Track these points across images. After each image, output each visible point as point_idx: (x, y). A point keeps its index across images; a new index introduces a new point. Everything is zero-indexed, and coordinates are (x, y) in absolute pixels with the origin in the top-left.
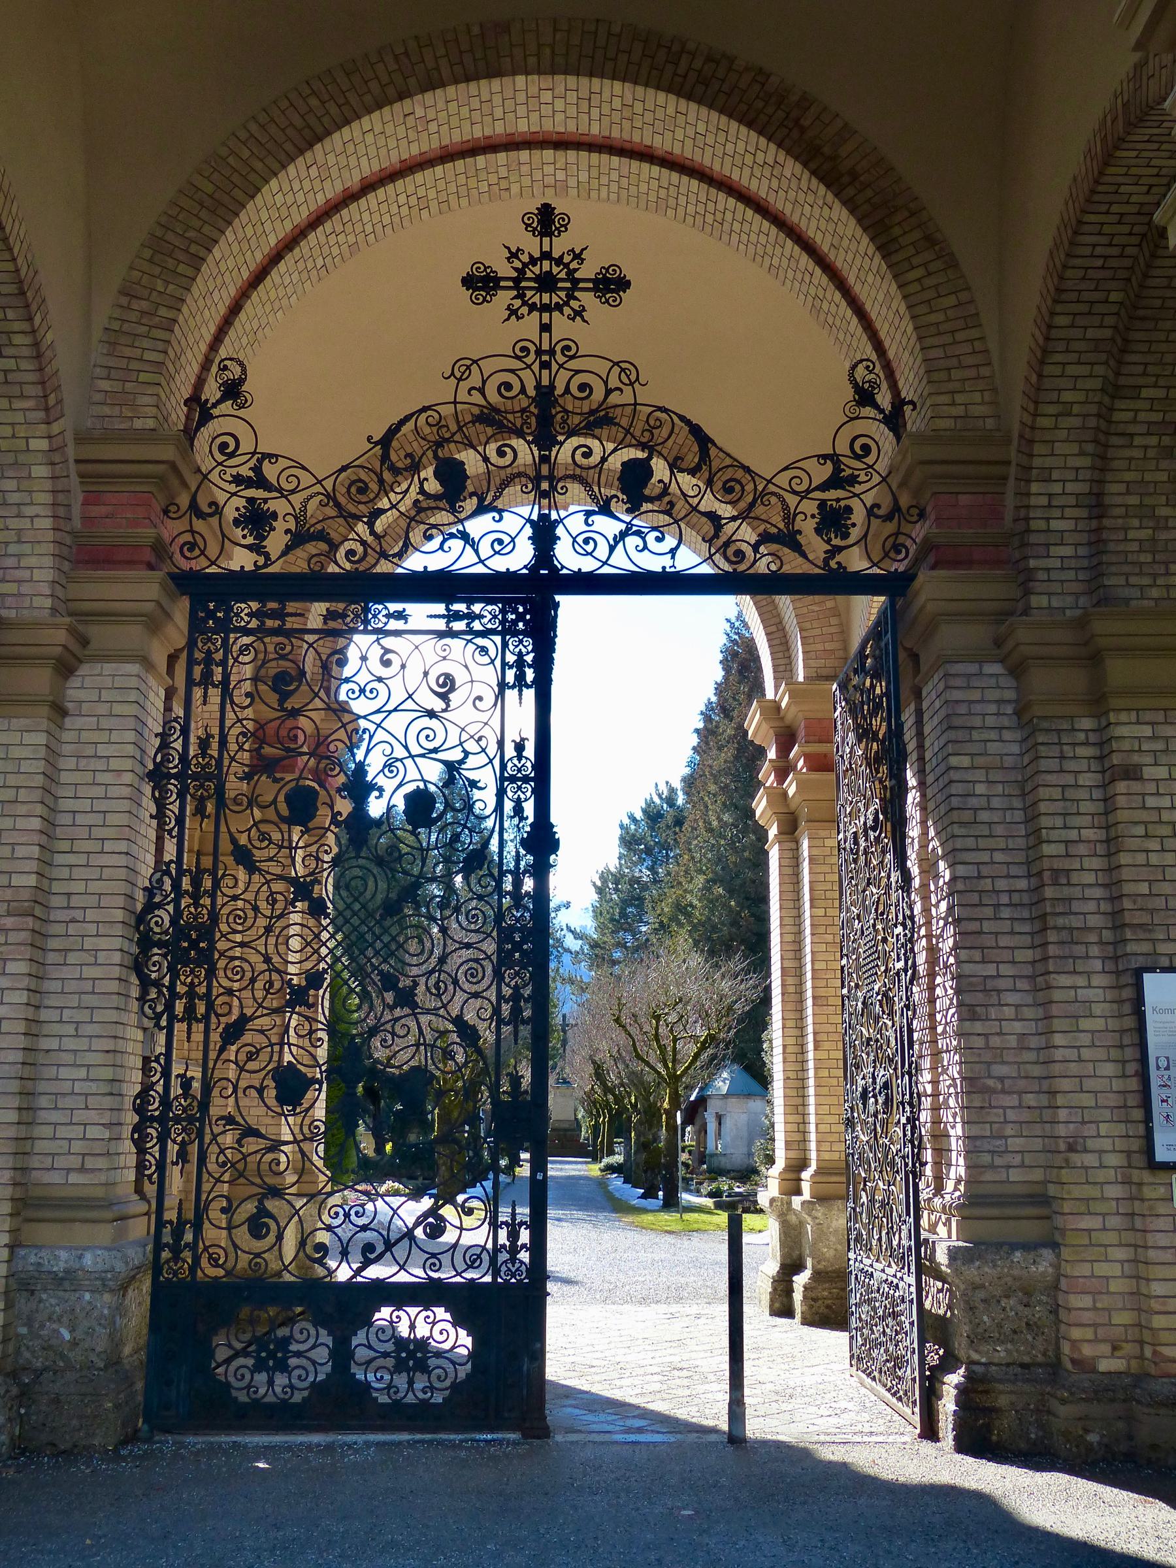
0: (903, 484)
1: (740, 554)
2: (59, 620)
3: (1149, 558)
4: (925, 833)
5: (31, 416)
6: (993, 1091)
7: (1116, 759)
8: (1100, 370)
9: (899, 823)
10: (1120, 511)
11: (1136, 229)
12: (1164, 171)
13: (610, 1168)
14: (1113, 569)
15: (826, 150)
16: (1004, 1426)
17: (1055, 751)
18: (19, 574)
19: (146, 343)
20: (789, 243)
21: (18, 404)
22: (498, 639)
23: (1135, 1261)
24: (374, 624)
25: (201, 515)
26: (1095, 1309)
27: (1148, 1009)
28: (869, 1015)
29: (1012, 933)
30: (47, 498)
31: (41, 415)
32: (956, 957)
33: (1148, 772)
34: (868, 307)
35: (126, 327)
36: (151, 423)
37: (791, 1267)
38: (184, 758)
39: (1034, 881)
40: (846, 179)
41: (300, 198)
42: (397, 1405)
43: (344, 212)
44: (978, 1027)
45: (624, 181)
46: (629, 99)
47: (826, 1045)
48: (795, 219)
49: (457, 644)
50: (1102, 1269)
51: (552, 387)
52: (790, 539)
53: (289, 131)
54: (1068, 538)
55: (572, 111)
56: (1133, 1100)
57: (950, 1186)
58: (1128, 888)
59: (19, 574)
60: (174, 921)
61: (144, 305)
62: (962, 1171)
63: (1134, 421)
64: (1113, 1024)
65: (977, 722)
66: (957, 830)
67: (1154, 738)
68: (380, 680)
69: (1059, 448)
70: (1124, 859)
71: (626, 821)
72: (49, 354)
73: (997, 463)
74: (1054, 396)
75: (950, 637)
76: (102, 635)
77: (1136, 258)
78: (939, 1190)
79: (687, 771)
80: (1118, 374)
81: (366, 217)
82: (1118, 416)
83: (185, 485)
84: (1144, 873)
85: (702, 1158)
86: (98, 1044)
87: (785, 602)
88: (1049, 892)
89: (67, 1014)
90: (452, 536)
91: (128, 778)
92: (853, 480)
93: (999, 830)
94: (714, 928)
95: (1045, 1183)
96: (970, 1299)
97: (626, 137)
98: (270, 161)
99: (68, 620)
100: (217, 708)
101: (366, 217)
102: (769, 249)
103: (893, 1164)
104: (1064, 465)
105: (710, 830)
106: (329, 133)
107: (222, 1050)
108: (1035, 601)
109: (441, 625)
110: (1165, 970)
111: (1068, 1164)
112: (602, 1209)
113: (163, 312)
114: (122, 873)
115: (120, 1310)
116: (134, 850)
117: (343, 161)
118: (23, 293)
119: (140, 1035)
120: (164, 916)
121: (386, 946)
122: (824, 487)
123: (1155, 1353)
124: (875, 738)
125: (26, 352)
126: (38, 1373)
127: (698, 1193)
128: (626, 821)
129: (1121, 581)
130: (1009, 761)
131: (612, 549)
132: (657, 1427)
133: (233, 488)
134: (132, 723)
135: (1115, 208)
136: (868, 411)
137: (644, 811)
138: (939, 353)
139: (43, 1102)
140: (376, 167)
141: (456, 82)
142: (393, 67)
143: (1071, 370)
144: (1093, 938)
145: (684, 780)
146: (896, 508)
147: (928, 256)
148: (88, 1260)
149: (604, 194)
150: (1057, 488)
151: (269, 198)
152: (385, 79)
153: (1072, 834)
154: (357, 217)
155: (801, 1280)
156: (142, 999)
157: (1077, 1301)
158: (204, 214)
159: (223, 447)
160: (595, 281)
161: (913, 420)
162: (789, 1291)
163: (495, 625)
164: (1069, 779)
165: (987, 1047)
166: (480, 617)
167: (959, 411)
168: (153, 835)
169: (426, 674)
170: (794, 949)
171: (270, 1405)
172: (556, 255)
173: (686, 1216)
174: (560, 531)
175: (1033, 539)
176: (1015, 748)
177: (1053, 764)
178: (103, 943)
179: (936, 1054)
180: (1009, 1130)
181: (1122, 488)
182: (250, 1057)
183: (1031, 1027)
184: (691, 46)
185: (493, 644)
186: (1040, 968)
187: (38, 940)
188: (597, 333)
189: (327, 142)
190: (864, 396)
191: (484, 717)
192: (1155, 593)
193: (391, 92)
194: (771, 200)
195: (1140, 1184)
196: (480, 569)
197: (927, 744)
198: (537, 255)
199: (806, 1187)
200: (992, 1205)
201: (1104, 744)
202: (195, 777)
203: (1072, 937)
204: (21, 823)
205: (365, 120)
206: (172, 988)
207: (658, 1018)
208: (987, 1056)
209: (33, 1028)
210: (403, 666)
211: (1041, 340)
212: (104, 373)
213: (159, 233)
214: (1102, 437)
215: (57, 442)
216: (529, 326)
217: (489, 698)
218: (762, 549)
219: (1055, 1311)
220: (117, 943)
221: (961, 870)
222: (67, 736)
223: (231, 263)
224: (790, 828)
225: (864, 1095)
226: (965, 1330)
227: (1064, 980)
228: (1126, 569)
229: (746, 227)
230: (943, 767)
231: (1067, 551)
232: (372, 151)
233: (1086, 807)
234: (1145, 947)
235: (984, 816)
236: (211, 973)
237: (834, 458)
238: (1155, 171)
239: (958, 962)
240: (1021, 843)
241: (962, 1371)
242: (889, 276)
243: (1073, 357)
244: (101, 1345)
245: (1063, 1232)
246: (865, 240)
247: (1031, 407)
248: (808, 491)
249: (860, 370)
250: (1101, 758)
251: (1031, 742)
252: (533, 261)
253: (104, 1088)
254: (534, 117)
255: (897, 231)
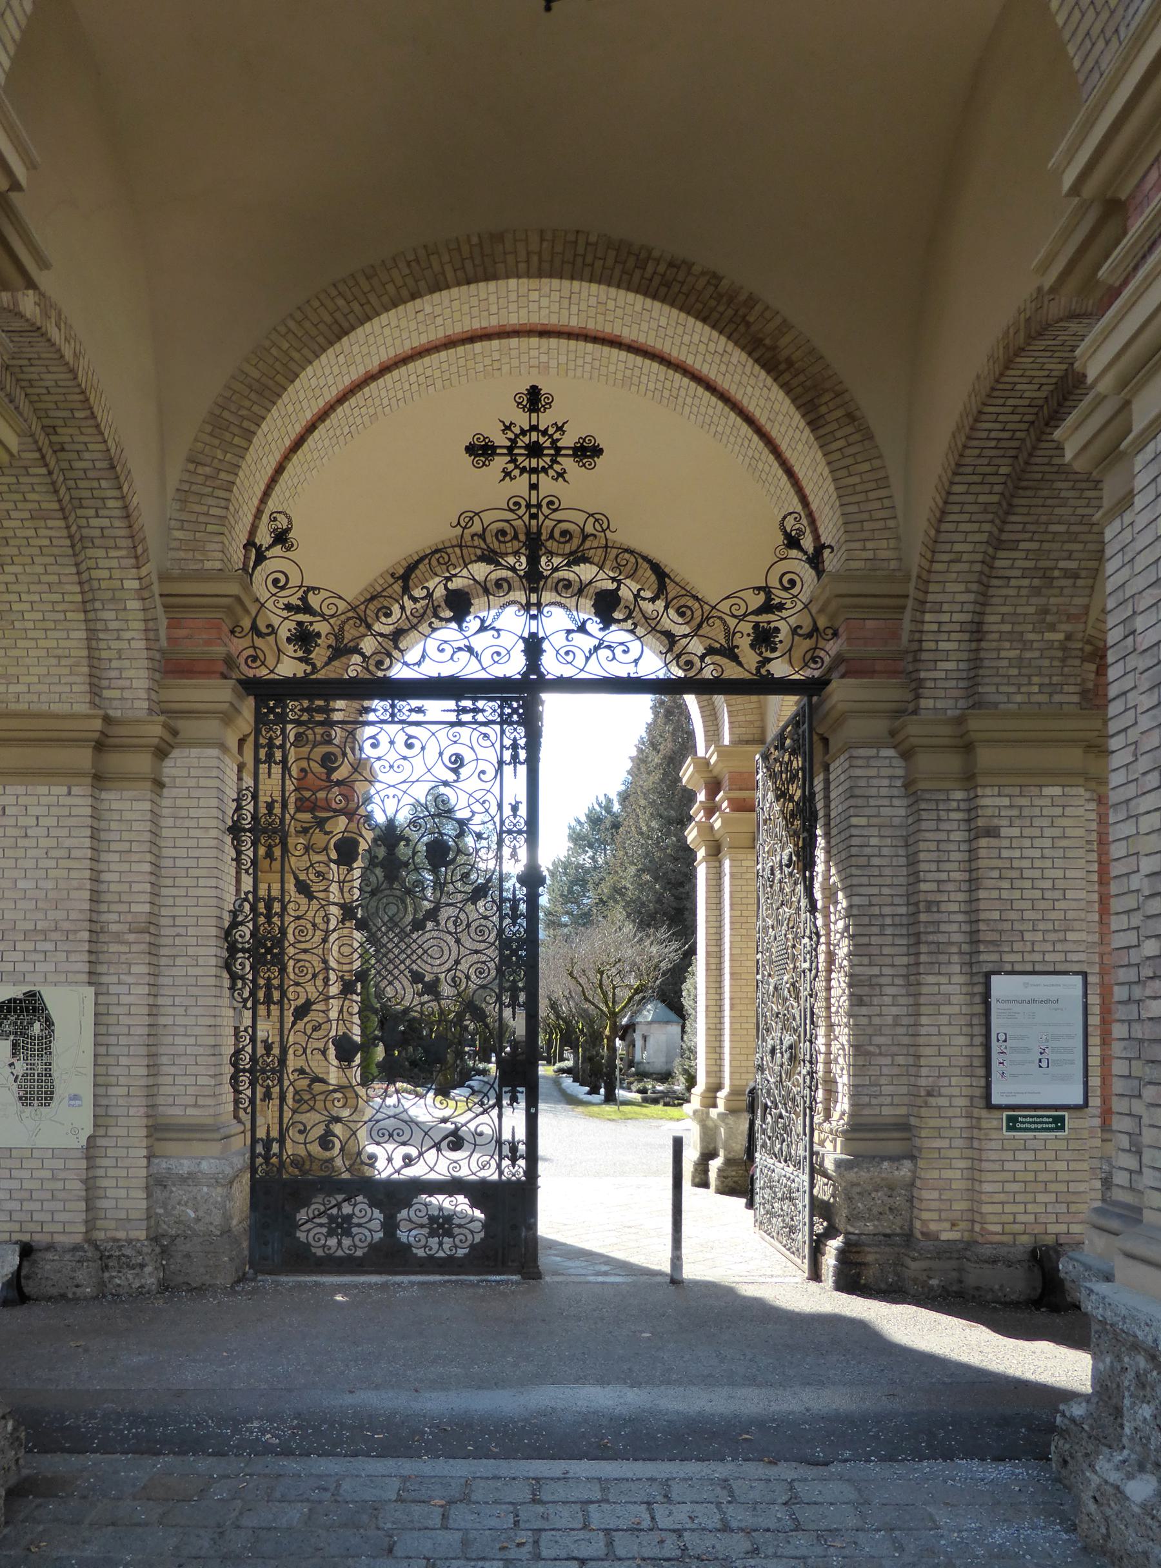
0: (821, 611)
1: (690, 664)
2: (155, 718)
7: (980, 822)
8: (987, 527)
9: (808, 863)
11: (1026, 418)
12: (1054, 373)
13: (562, 1071)
14: (987, 680)
15: (767, 342)
16: (869, 1275)
17: (933, 815)
18: (120, 683)
19: (211, 501)
20: (733, 415)
21: (112, 553)
22: (497, 728)
23: (972, 1169)
24: (399, 717)
25: (260, 634)
26: (940, 1200)
27: (993, 1000)
28: (779, 997)
29: (893, 945)
31: (133, 561)
32: (850, 961)
33: (1004, 832)
35: (194, 488)
36: (218, 565)
37: (708, 1155)
38: (255, 817)
39: (912, 909)
40: (782, 367)
41: (330, 380)
43: (366, 390)
44: (864, 1010)
45: (597, 364)
46: (603, 298)
47: (740, 1007)
48: (739, 397)
49: (464, 732)
51: (539, 533)
52: (730, 653)
53: (321, 326)
54: (953, 656)
55: (555, 307)
56: (977, 1062)
57: (836, 1116)
58: (982, 916)
59: (120, 683)
60: (253, 935)
61: (208, 470)
62: (846, 1107)
63: (1012, 567)
65: (873, 792)
66: (854, 871)
67: (1011, 806)
68: (405, 758)
69: (950, 587)
70: (982, 894)
71: (573, 824)
72: (135, 513)
73: (898, 596)
74: (948, 547)
75: (855, 728)
76: (187, 728)
77: (1023, 440)
78: (828, 1117)
79: (623, 788)
80: (1001, 531)
81: (383, 393)
83: (247, 611)
84: (998, 905)
85: (631, 1064)
86: (201, 1021)
87: (719, 700)
88: (923, 917)
89: (177, 1001)
90: (460, 649)
91: (214, 833)
92: (781, 607)
94: (643, 904)
95: (908, 1115)
97: (599, 328)
98: (305, 351)
99: (162, 718)
101: (383, 393)
102: (715, 419)
103: (794, 1100)
104: (953, 598)
105: (642, 834)
106: (353, 328)
107: (294, 1024)
108: (923, 703)
109: (452, 717)
110: (1007, 973)
111: (926, 1105)
112: (558, 1102)
113: (223, 475)
115: (229, 1197)
116: (221, 884)
117: (365, 350)
118: (113, 467)
119: (231, 1013)
120: (246, 930)
122: (759, 611)
123: (982, 1229)
125: (117, 513)
126: (174, 1238)
127: (629, 1089)
128: (573, 824)
129: (993, 689)
130: (896, 821)
131: (587, 659)
132: (618, 1271)
133: (285, 614)
134: (214, 793)
135: (1011, 402)
136: (794, 553)
137: (587, 816)
140: (392, 354)
141: (459, 284)
142: (406, 271)
143: (963, 527)
144: (954, 949)
145: (619, 794)
146: (815, 629)
147: (849, 430)
148: (204, 1165)
149: (579, 374)
150: (945, 618)
151: (305, 381)
152: (400, 283)
153: (943, 876)
155: (715, 1165)
156: (232, 988)
157: (925, 1194)
158: (253, 396)
159: (276, 582)
160: (575, 449)
161: (830, 561)
162: (706, 1171)
163: (496, 717)
164: (943, 836)
165: (870, 1024)
166: (483, 711)
168: (233, 872)
169: (441, 754)
170: (716, 939)
171: (340, 1258)
172: (542, 428)
173: (623, 1108)
174: (546, 645)
175: (924, 656)
176: (902, 812)
177: (932, 825)
178: (202, 951)
179: (830, 1026)
180: (883, 1081)
181: (998, 618)
182: (315, 1029)
184: (656, 254)
185: (493, 731)
186: (913, 970)
187: (153, 950)
188: (576, 491)
189: (352, 335)
190: (792, 542)
191: (487, 786)
192: (1019, 698)
193: (405, 293)
195: (979, 1119)
196: (482, 675)
197: (833, 805)
199: (721, 1103)
200: (871, 1130)
201: (972, 811)
203: (938, 949)
205: (384, 317)
206: (254, 981)
207: (602, 973)
208: (870, 1031)
209: (153, 1010)
210: (423, 748)
211: (941, 504)
212: (178, 524)
213: (217, 412)
214: (985, 580)
215: (145, 582)
216: (521, 484)
217: (491, 772)
218: (708, 660)
219: (911, 1200)
220: (213, 951)
221: (856, 900)
222: (165, 803)
223: (276, 434)
224: (715, 851)
225: (773, 1051)
226: (844, 1212)
227: (930, 979)
228: (997, 680)
229: (697, 401)
230: (845, 824)
231: (951, 666)
232: (389, 341)
233: (955, 856)
234: (994, 957)
235: (875, 861)
237: (766, 590)
238: (1046, 373)
239: (852, 966)
241: (841, 1238)
243: (966, 517)
244: (217, 1219)
245: (920, 1149)
247: (929, 555)
248: (745, 615)
251: (915, 808)
252: (523, 432)
253: (210, 1051)
254: (523, 312)
255: (823, 410)
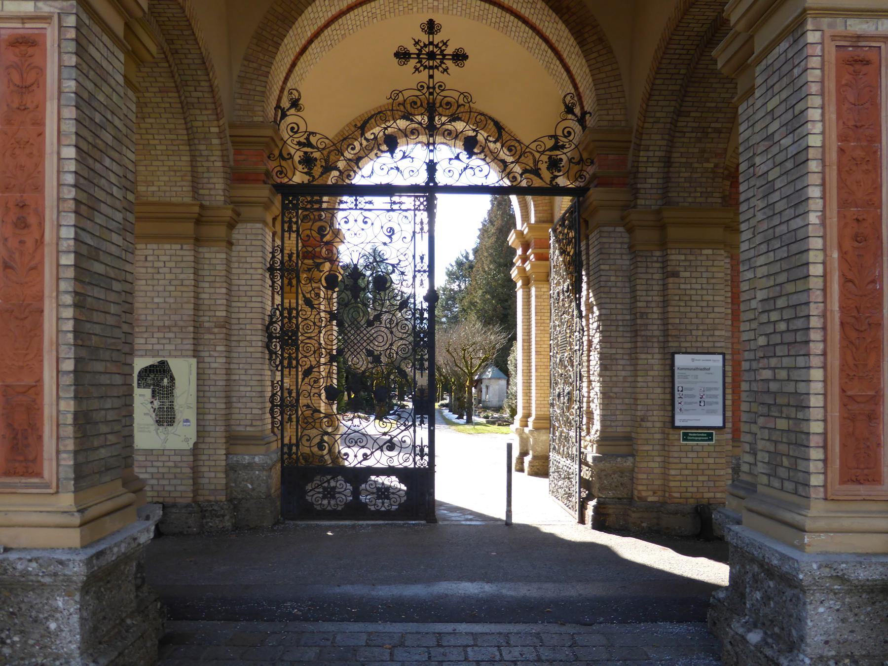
3: (688, 185)
4: (588, 294)
5: (210, 117)
6: (612, 398)
7: (669, 269)
8: (673, 103)
10: (677, 165)
17: (644, 265)
19: (256, 83)
21: (204, 112)
25: (284, 159)
27: (676, 368)
29: (623, 337)
30: (219, 153)
31: (215, 117)
33: (682, 274)
34: (571, 68)
36: (261, 119)
37: (524, 454)
38: (282, 262)
39: (633, 317)
41: (321, 14)
42: (378, 511)
43: (340, 20)
44: (608, 373)
45: (464, 7)
48: (541, 27)
50: (652, 465)
51: (434, 103)
52: (536, 172)
56: (667, 403)
57: (593, 432)
58: (671, 321)
61: (255, 65)
63: (686, 126)
64: (661, 373)
65: (612, 251)
67: (685, 260)
69: (653, 137)
70: (670, 309)
72: (216, 89)
76: (245, 211)
78: (588, 433)
80: (681, 106)
82: (679, 124)
83: (277, 146)
84: (678, 315)
85: (480, 402)
86: (254, 378)
88: (639, 321)
91: (260, 271)
93: (619, 296)
94: (486, 312)
95: (630, 432)
96: (599, 473)
99: (232, 206)
100: (295, 242)
101: (349, 22)
102: (528, 40)
103: (570, 423)
105: (485, 272)
108: (639, 202)
109: (388, 207)
110: (683, 353)
111: (641, 426)
113: (263, 68)
114: (260, 310)
116: (264, 300)
118: (204, 63)
119: (269, 373)
121: (368, 338)
124: (568, 254)
130: (624, 268)
133: (297, 147)
134: (260, 248)
135: (686, 33)
136: (570, 116)
138: (603, 92)
139: (234, 399)
143: (661, 103)
144: (655, 340)
146: (581, 160)
148: (257, 459)
150: (651, 154)
154: (345, 22)
156: (270, 359)
157: (641, 476)
161: (590, 121)
164: (649, 276)
167: (611, 118)
168: (270, 293)
171: (329, 511)
172: (435, 43)
173: (477, 427)
175: (640, 175)
176: (628, 262)
178: (254, 338)
180: (618, 412)
181: (678, 155)
183: (629, 373)
187: (228, 337)
190: (569, 110)
194: (530, 18)
197: (591, 258)
198: (427, 43)
199: (530, 424)
201: (665, 263)
202: (287, 270)
204: (218, 291)
206: (282, 355)
209: (229, 372)
216: (424, 75)
219: (632, 479)
220: (260, 338)
221: (604, 311)
222: (234, 254)
223: (292, 45)
224: (527, 284)
226: (597, 486)
227: (643, 356)
229: (518, 29)
234: (676, 344)
235: (613, 290)
236: (297, 349)
237: (555, 137)
239: (601, 348)
240: (628, 301)
241: (596, 500)
242: (582, 56)
243: (661, 98)
245: (637, 451)
246: (572, 39)
247: (643, 119)
248: (544, 151)
249: (568, 98)
250: (663, 268)
255: (586, 35)
